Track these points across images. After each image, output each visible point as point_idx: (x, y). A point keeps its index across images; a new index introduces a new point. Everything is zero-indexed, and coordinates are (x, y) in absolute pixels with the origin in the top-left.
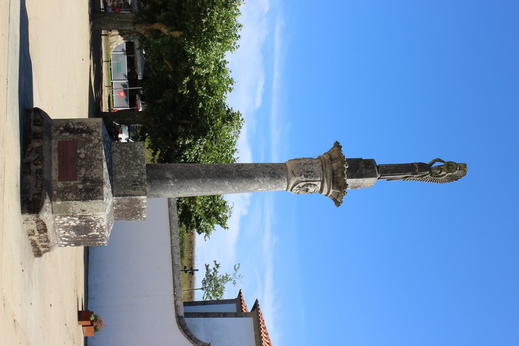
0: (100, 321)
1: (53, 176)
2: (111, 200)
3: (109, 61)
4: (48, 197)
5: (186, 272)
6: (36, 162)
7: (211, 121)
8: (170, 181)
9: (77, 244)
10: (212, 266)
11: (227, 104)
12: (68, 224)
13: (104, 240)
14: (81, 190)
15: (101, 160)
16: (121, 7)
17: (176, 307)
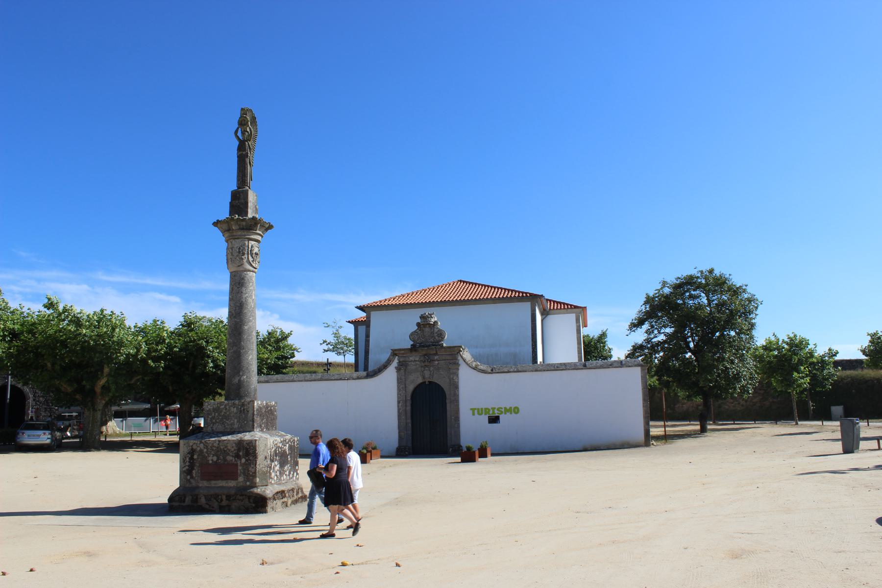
0: (368, 445)
1: (232, 485)
2: (258, 433)
3: (131, 435)
4: (252, 490)
5: (329, 369)
6: (219, 501)
7: (191, 341)
8: (242, 379)
9: (297, 464)
10: (325, 347)
11: (176, 327)
12: (278, 472)
13: (294, 440)
14: (246, 460)
15: (219, 441)
16: (80, 422)
17: (358, 378)
